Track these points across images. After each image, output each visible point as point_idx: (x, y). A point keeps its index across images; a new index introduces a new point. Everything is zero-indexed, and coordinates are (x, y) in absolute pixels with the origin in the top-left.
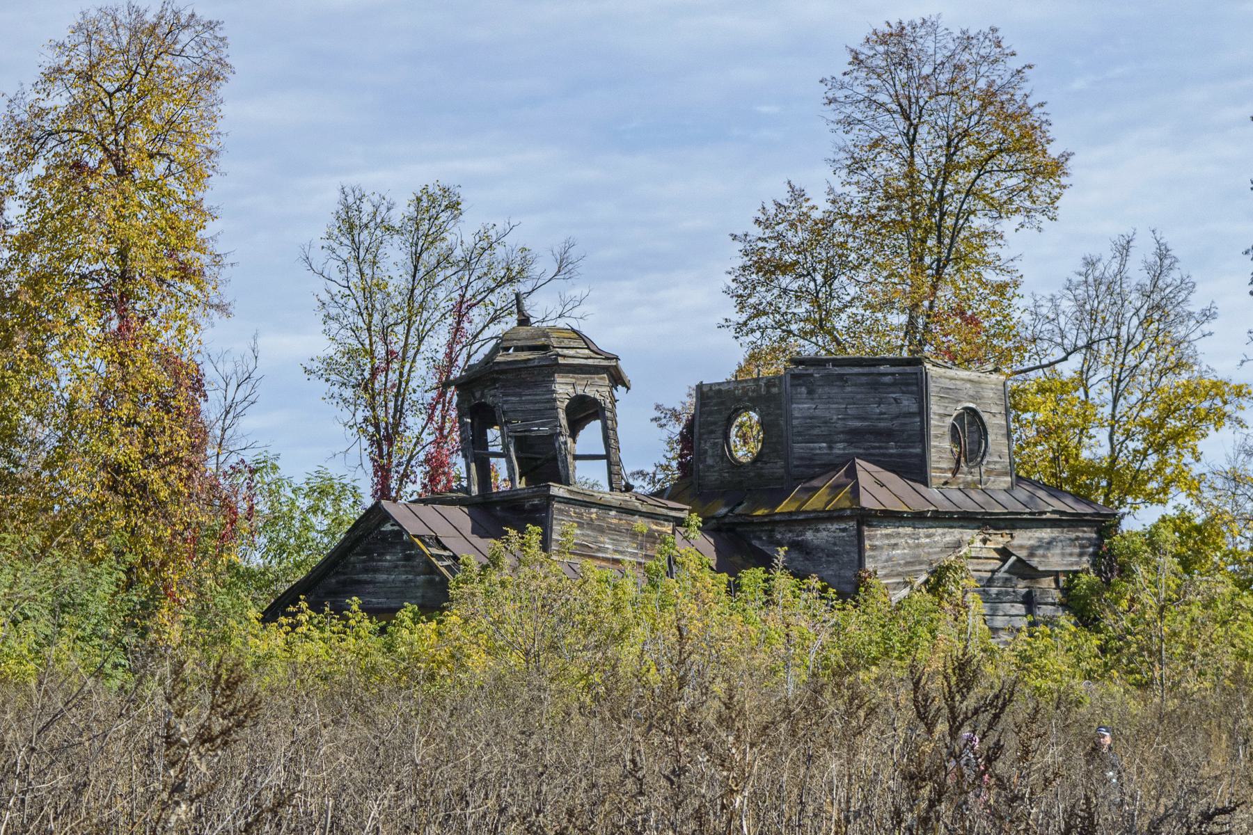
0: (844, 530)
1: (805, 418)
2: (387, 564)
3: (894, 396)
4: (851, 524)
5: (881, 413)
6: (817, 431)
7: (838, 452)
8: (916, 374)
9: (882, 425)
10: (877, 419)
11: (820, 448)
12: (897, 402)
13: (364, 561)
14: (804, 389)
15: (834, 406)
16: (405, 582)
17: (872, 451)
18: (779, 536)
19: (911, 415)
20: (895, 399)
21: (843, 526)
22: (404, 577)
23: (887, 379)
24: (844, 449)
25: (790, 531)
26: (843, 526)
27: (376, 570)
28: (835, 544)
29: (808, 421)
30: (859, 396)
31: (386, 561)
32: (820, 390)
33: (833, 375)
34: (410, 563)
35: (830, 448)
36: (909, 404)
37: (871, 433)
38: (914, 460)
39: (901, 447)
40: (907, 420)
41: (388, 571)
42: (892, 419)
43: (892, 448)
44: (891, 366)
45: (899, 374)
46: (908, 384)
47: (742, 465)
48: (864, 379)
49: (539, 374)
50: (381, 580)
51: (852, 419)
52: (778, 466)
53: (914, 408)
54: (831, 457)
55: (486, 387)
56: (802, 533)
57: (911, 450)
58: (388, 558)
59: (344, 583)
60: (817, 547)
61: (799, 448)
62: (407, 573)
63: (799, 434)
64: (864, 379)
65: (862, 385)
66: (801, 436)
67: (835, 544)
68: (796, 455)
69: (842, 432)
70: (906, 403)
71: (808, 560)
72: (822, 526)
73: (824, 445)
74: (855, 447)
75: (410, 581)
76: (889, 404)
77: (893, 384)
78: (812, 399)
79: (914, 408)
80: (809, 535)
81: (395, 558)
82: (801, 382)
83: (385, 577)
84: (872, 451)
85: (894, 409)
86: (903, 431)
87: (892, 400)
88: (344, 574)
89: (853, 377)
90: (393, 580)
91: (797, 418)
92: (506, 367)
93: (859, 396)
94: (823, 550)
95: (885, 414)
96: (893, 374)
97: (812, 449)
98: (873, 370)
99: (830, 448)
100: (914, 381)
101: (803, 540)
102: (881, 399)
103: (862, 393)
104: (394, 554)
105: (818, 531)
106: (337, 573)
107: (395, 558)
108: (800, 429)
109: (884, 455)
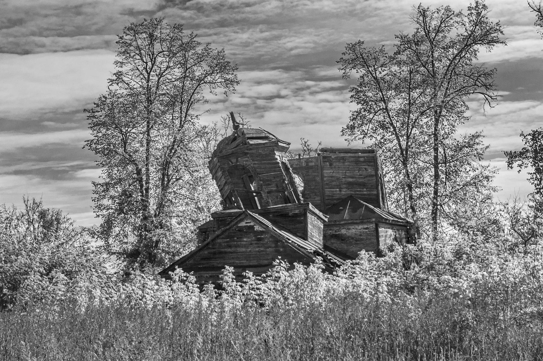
0: (367, 228)
1: (329, 177)
2: (245, 243)
3: (365, 167)
4: (371, 225)
6: (334, 183)
7: (343, 193)
11: (336, 191)
12: (366, 170)
13: (227, 242)
15: (341, 171)
16: (259, 251)
17: (357, 193)
19: (372, 176)
20: (365, 169)
21: (366, 226)
22: (257, 249)
23: (362, 159)
24: (346, 191)
25: (330, 230)
26: (366, 226)
27: (237, 246)
28: (361, 235)
29: (330, 178)
30: (351, 167)
31: (244, 241)
33: (339, 157)
34: (262, 242)
35: (340, 191)
36: (371, 171)
37: (356, 184)
38: (374, 197)
39: (368, 191)
40: (370, 179)
41: (245, 246)
42: (364, 178)
45: (367, 157)
46: (370, 162)
50: (241, 251)
51: (348, 178)
52: (316, 199)
53: (373, 173)
54: (341, 196)
56: (339, 230)
58: (245, 240)
59: (214, 253)
60: (349, 237)
62: (259, 247)
63: (327, 184)
64: (352, 159)
65: (352, 162)
66: (328, 185)
67: (361, 235)
68: (326, 194)
69: (345, 184)
70: (370, 170)
71: (342, 243)
72: (351, 227)
73: (338, 189)
74: (351, 191)
75: (262, 251)
76: (363, 171)
77: (364, 162)
79: (373, 173)
80: (343, 231)
81: (250, 240)
82: (326, 160)
83: (244, 250)
84: (357, 193)
85: (364, 173)
88: (214, 249)
90: (250, 251)
91: (326, 177)
93: (351, 167)
94: (353, 238)
95: (361, 175)
99: (340, 191)
101: (339, 234)
102: (359, 168)
104: (249, 238)
105: (349, 229)
106: (209, 248)
107: (250, 240)
108: (327, 182)
109: (361, 195)
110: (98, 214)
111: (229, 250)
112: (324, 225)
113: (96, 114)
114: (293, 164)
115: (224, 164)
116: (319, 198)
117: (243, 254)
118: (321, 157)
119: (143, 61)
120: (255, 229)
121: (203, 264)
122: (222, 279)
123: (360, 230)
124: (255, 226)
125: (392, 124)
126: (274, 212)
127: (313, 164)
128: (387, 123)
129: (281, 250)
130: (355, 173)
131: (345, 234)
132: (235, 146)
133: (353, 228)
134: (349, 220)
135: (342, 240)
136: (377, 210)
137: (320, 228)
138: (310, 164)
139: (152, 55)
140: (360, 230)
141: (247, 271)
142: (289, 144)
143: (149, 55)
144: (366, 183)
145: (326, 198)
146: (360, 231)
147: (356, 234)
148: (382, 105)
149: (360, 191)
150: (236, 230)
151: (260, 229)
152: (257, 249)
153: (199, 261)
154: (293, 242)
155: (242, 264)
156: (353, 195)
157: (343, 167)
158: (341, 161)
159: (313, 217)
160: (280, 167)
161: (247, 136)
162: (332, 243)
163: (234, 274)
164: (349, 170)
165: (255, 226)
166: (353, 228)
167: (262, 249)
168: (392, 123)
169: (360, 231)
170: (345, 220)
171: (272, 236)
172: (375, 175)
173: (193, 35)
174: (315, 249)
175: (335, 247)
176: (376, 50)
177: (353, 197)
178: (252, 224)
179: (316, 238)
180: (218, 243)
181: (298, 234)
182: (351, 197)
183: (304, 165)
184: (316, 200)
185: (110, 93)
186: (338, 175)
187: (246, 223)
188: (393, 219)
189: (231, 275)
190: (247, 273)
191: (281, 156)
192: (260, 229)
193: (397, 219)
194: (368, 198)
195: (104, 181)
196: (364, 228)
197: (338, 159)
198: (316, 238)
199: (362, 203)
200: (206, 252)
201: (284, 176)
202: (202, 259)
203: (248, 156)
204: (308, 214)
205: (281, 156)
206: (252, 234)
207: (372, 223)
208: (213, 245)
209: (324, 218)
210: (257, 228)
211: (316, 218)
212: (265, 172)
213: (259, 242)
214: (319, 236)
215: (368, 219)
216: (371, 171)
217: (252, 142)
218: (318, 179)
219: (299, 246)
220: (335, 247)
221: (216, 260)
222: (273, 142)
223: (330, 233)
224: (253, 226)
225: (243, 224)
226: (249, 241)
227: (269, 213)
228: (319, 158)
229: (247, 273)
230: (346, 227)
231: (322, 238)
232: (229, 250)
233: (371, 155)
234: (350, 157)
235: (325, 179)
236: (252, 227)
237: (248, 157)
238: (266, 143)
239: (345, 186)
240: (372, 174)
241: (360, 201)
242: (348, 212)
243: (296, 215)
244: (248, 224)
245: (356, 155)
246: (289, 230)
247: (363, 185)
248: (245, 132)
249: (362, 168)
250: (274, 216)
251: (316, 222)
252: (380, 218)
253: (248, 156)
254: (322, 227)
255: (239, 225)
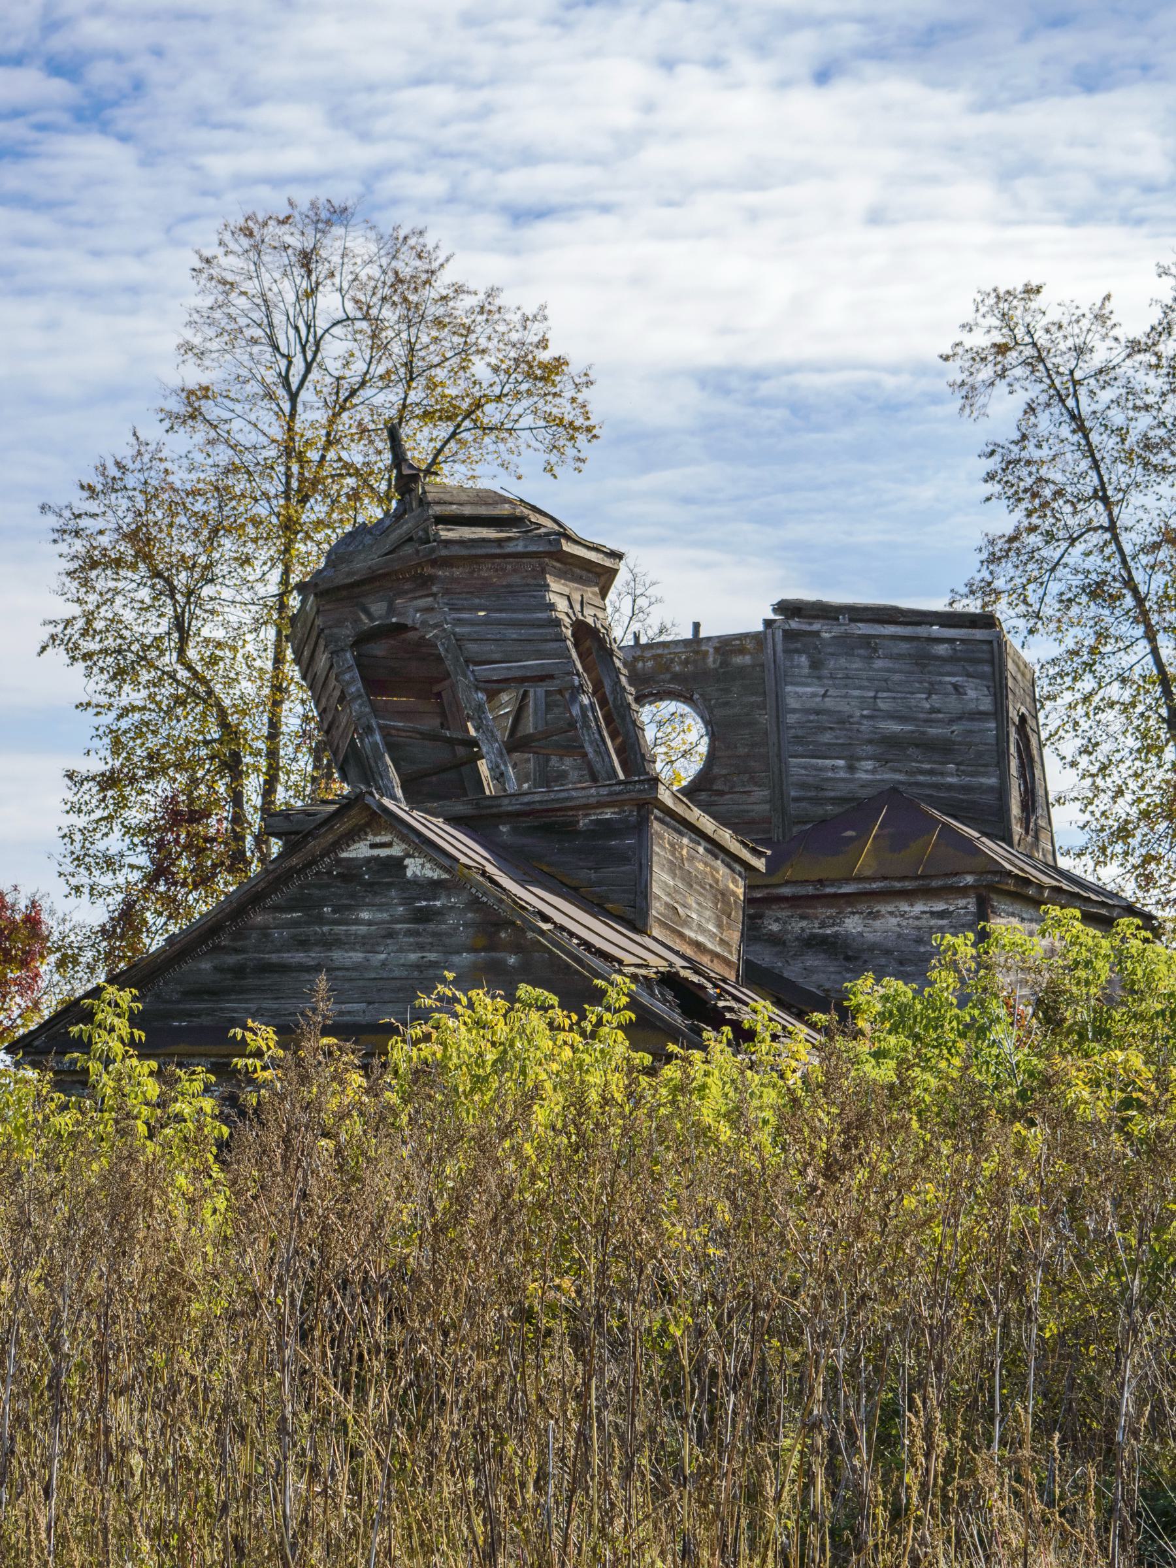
2: (363, 929)
3: (953, 680)
4: (961, 903)
5: (934, 710)
6: (827, 738)
7: (864, 776)
8: (990, 642)
9: (934, 731)
10: (926, 721)
11: (834, 768)
13: (295, 923)
14: (803, 660)
15: (857, 693)
16: (417, 966)
17: (921, 778)
18: (775, 927)
19: (981, 715)
20: (956, 687)
21: (939, 906)
22: (413, 957)
23: (942, 649)
24: (873, 771)
25: (803, 917)
26: (939, 906)
27: (330, 943)
30: (896, 677)
31: (358, 922)
32: (831, 664)
34: (431, 927)
35: (851, 768)
37: (917, 746)
38: (990, 799)
40: (975, 726)
41: (368, 944)
43: (951, 775)
44: (942, 626)
45: (962, 641)
46: (975, 661)
47: (285, 845)
48: (904, 647)
49: (515, 571)
50: (348, 963)
53: (986, 705)
54: (851, 786)
55: (401, 593)
56: (835, 920)
57: (983, 780)
58: (365, 915)
59: (239, 971)
60: (872, 947)
61: (798, 767)
62: (421, 947)
64: (904, 647)
65: (898, 657)
68: (794, 779)
69: (870, 742)
70: (972, 694)
72: (884, 908)
73: (841, 763)
74: (895, 770)
76: (947, 694)
77: (952, 659)
78: (819, 678)
79: (986, 705)
80: (853, 925)
81: (385, 916)
82: (799, 645)
83: (357, 956)
84: (921, 778)
85: (953, 704)
86: (970, 745)
87: (950, 688)
88: (236, 951)
89: (887, 642)
90: (384, 964)
91: (794, 711)
92: (464, 552)
93: (896, 677)
94: (887, 952)
95: (939, 711)
96: (951, 641)
97: (820, 769)
98: (922, 631)
99: (851, 768)
100: (986, 656)
101: (836, 935)
102: (931, 684)
103: (901, 672)
104: (381, 907)
105: (875, 916)
106: (217, 949)
107: (385, 916)
108: (800, 732)
110: (73, 881)
111: (299, 957)
112: (749, 888)
113: (84, 522)
114: (672, 661)
115: (339, 623)
116: (760, 794)
117: (354, 974)
118: (779, 634)
119: (276, 348)
120: (409, 873)
121: (189, 1014)
122: (84, 1045)
123: (918, 918)
124: (407, 861)
125: (1130, 583)
126: (518, 814)
127: (747, 660)
128: (1115, 579)
129: (512, 960)
130: (913, 703)
131: (861, 934)
132: (387, 548)
133: (891, 913)
134: (874, 879)
135: (848, 959)
136: (988, 846)
137: (723, 895)
138: (738, 660)
139: (309, 327)
140: (918, 918)
141: (250, 1023)
142: (617, 556)
143: (297, 328)
144: (954, 743)
145: (793, 793)
146: (916, 923)
147: (899, 935)
148: (1096, 513)
149: (931, 772)
150: (329, 873)
151: (436, 874)
152: (413, 957)
153: (179, 1002)
154: (562, 928)
155: (347, 1018)
156: (902, 788)
157: (864, 674)
158: (862, 652)
159: (685, 841)
160: (564, 640)
161: (437, 510)
162: (809, 971)
163: (135, 1020)
164: (889, 690)
165: (407, 861)
166: (891, 913)
167: (433, 956)
168: (1131, 579)
169: (916, 923)
170: (859, 879)
171: (474, 903)
172: (995, 713)
173: (439, 253)
174: (663, 967)
175: (819, 987)
176: (1079, 312)
177: (900, 793)
178: (397, 851)
179: (701, 929)
180: (253, 928)
181: (609, 906)
182: (893, 793)
183: (711, 661)
184: (752, 799)
185: (139, 453)
186: (843, 707)
187: (373, 846)
188: (1055, 883)
189: (122, 1026)
190: (251, 1030)
191: (576, 597)
192: (429, 874)
193: (1077, 890)
194: (962, 801)
195: (100, 767)
196: (932, 913)
197: (847, 645)
198: (701, 929)
199: (932, 817)
200: (206, 965)
201: (578, 674)
202: (189, 994)
203: (435, 589)
204: (656, 826)
205: (576, 597)
206: (393, 893)
207: (963, 891)
208: (238, 935)
209: (745, 855)
210: (415, 867)
211: (701, 850)
212: (496, 656)
213: (421, 927)
214: (719, 926)
215: (947, 875)
216: (977, 696)
217: (446, 534)
218: (765, 718)
219: (588, 946)
220: (819, 987)
221: (246, 1001)
222: (539, 536)
223: (803, 929)
224: (402, 859)
225: (360, 850)
226: (383, 922)
227: (493, 816)
228: (769, 637)
229: (251, 1030)
230: (863, 907)
231: (735, 936)
232: (299, 957)
233: (979, 634)
234: (894, 638)
235: (791, 719)
236: (396, 865)
237: (434, 595)
238: (509, 539)
239: (869, 749)
240: (982, 708)
241: (923, 806)
242: (875, 849)
243: (606, 829)
244: (383, 852)
245: (922, 631)
246: (576, 889)
247: (943, 749)
248: (430, 497)
249: (940, 683)
250: (515, 830)
251: (701, 866)
252: (995, 873)
253: (435, 589)
254: (740, 891)
255: (344, 855)
